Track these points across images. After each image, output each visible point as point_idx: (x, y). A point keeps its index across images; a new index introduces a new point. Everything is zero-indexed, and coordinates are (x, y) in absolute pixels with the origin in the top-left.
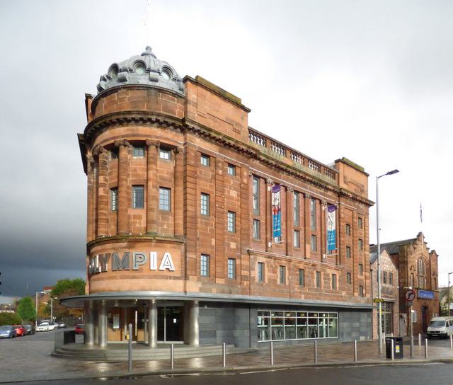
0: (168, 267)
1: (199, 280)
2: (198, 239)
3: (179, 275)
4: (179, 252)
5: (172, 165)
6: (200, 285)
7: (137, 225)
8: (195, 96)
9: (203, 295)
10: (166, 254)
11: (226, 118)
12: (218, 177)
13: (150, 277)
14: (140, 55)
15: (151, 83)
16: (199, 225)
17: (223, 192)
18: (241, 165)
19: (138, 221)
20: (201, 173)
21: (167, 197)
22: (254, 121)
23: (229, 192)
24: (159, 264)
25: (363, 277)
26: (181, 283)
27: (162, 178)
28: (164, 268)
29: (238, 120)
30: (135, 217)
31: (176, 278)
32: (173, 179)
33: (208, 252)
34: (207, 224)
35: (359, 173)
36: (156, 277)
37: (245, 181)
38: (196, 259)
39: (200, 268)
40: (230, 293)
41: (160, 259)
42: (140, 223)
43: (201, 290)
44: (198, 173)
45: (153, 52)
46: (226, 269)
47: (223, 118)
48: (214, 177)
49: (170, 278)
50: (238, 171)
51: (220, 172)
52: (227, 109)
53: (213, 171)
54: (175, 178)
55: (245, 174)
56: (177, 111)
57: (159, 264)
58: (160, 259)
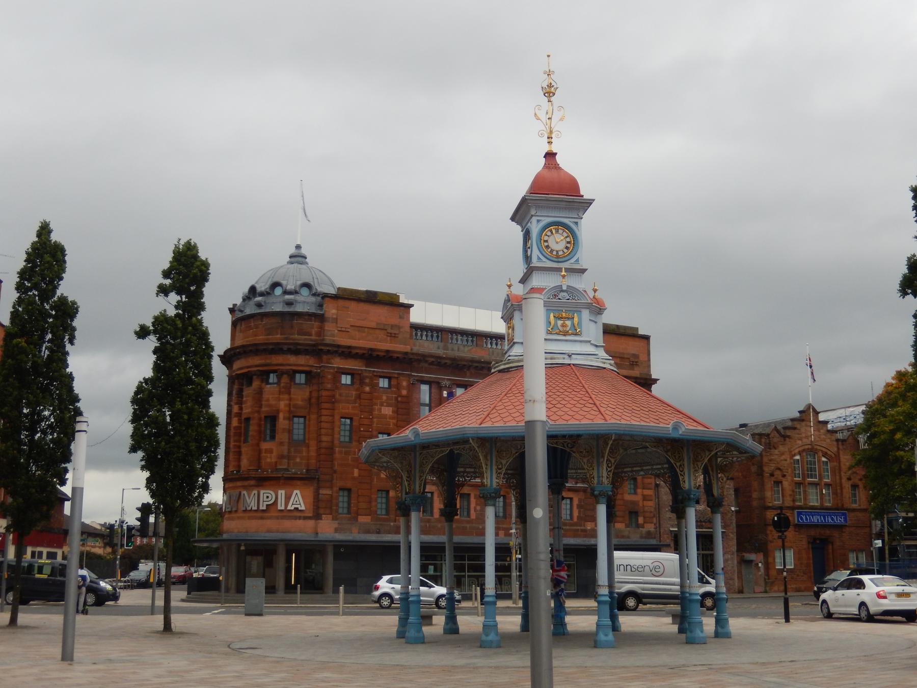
0: (296, 506)
1: (335, 519)
2: (335, 472)
3: (310, 515)
4: (310, 491)
5: (307, 390)
6: (335, 524)
7: (268, 460)
8: (334, 311)
9: (339, 537)
10: (819, 504)
11: (378, 324)
12: (363, 396)
13: (277, 518)
14: (286, 263)
15: (287, 309)
16: (337, 455)
17: (371, 412)
18: (399, 374)
19: (269, 455)
20: (340, 395)
21: (302, 426)
22: (585, 197)
23: (380, 410)
24: (286, 504)
25: (638, 498)
26: (311, 523)
27: (295, 406)
28: (292, 508)
29: (395, 321)
30: (267, 451)
31: (305, 518)
32: (308, 406)
33: (349, 484)
34: (347, 453)
35: (623, 340)
36: (283, 518)
37: (404, 392)
38: (332, 495)
39: (337, 505)
40: (378, 533)
41: (288, 498)
42: (271, 458)
43: (336, 530)
44: (337, 396)
45: (304, 251)
46: (373, 504)
47: (373, 325)
48: (359, 397)
49: (300, 518)
50: (394, 382)
51: (367, 389)
52: (378, 315)
53: (357, 390)
54: (310, 404)
55: (405, 384)
56: (313, 332)
57: (286, 504)
58: (288, 498)
